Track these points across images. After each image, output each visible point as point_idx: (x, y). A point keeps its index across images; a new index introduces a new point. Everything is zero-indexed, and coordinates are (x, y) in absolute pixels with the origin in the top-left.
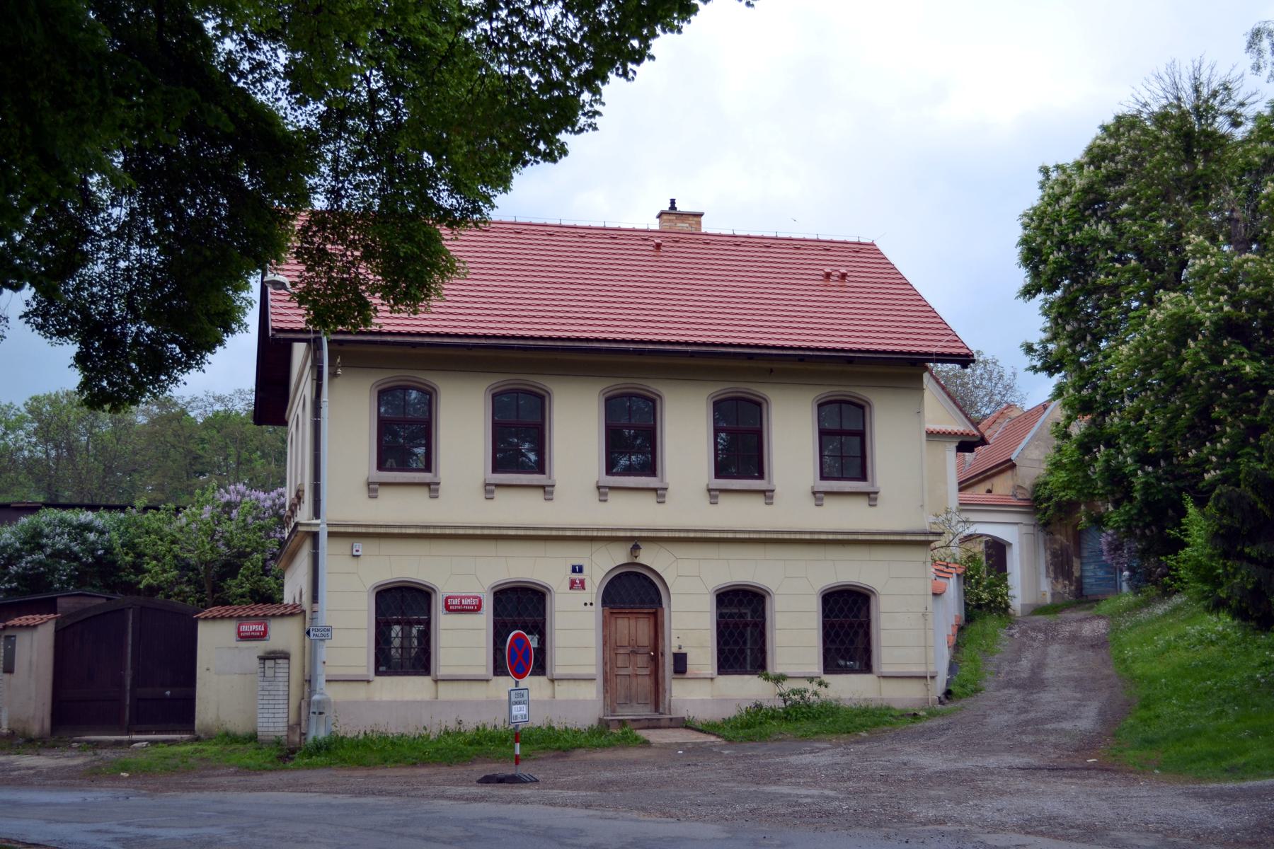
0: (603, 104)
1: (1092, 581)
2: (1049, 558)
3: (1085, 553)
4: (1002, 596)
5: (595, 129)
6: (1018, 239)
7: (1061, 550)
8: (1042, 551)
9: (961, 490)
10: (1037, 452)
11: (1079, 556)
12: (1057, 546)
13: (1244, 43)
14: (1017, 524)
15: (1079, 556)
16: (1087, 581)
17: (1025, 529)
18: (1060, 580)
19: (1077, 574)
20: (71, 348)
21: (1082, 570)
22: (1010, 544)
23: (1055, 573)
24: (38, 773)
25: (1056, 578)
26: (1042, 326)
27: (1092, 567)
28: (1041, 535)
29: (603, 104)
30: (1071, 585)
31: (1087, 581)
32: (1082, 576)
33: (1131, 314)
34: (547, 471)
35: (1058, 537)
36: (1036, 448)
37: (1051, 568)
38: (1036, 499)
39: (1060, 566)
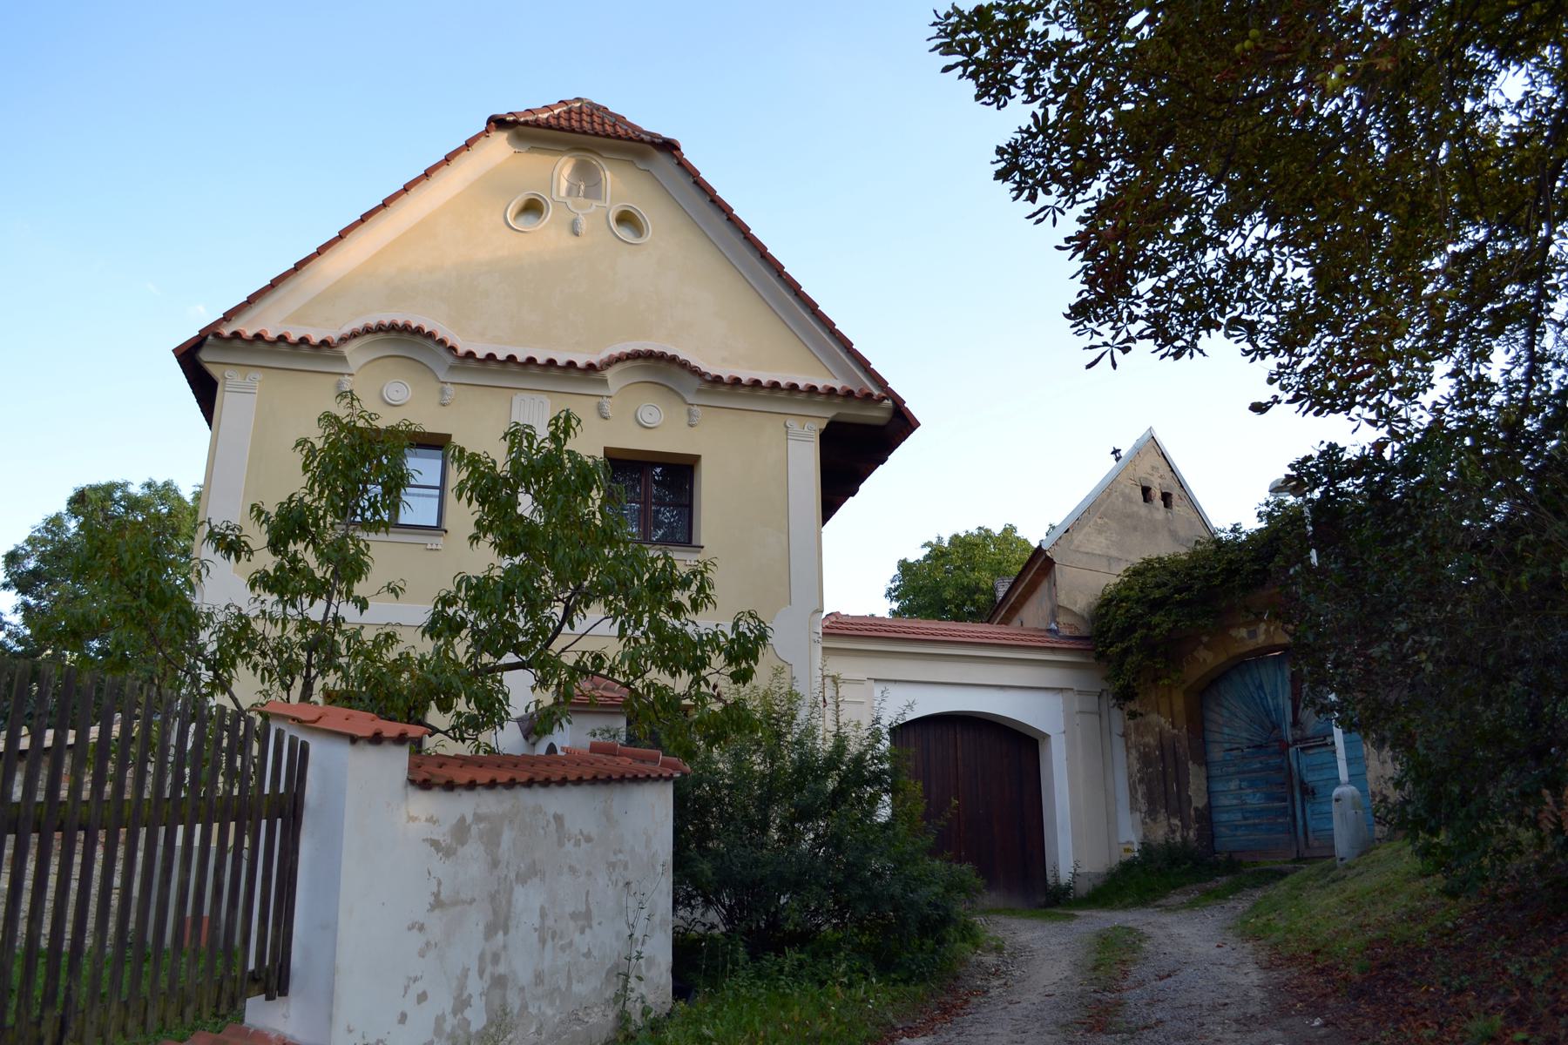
0: (960, 77)
1: (1237, 817)
2: (1136, 766)
3: (1216, 753)
4: (957, 978)
7: (1161, 747)
8: (1119, 744)
10: (1102, 540)
11: (1202, 759)
12: (1151, 740)
14: (1061, 690)
15: (1202, 759)
17: (1076, 703)
18: (1162, 817)
20: (426, 331)
21: (1210, 793)
22: (1046, 736)
23: (1151, 799)
24: (60, 875)
25: (1152, 813)
27: (1233, 785)
28: (1118, 719)
29: (960, 77)
30: (1185, 827)
31: (1224, 817)
32: (1209, 807)
34: (688, 463)
35: (1154, 718)
36: (1100, 532)
37: (1141, 790)
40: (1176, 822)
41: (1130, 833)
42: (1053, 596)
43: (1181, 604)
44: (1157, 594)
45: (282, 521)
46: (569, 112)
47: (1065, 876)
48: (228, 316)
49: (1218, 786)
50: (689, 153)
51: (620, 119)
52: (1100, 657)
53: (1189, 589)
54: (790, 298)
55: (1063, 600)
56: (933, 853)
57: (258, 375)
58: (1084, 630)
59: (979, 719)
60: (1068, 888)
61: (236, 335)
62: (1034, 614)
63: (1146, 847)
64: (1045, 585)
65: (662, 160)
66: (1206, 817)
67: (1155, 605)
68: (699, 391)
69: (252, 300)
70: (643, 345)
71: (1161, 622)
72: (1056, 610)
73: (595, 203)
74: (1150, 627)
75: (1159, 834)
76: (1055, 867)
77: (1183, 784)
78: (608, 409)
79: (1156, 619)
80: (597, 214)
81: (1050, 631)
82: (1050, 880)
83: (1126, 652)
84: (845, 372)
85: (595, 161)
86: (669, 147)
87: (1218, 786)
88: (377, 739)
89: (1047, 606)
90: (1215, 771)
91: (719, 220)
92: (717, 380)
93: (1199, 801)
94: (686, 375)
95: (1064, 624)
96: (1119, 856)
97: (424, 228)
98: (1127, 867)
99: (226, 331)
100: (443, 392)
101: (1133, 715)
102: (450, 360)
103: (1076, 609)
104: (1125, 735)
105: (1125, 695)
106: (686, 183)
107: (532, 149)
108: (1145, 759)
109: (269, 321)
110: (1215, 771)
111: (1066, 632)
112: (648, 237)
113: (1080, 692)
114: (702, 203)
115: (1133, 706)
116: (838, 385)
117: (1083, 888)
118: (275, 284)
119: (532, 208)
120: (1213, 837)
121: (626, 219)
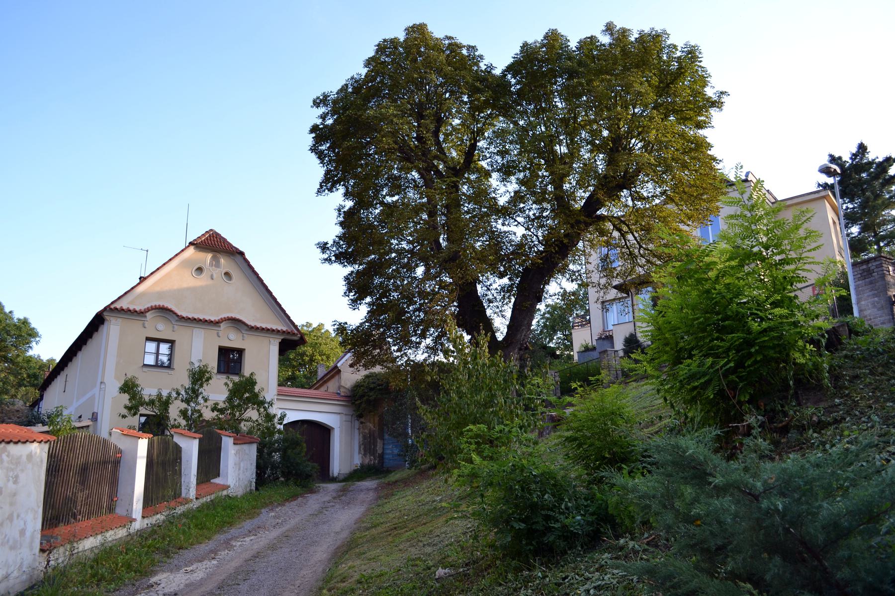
5: (831, 156)
6: (708, 61)
8: (357, 431)
9: (279, 385)
11: (382, 439)
12: (367, 431)
13: (449, 35)
15: (382, 439)
16: (387, 456)
17: (344, 418)
19: (380, 451)
22: (333, 428)
23: (365, 450)
25: (365, 455)
26: (15, 313)
27: (390, 447)
28: (357, 424)
30: (375, 459)
31: (387, 456)
32: (383, 453)
33: (572, 221)
35: (368, 424)
37: (362, 447)
38: (354, 396)
39: (368, 446)
40: (372, 457)
41: (357, 461)
42: (339, 381)
43: (380, 390)
44: (372, 386)
45: (18, 328)
46: (210, 236)
47: (336, 474)
48: (112, 303)
49: (386, 447)
50: (247, 256)
51: (225, 240)
52: (353, 403)
53: (382, 385)
54: (273, 302)
55: (343, 384)
56: (309, 460)
57: (120, 320)
58: (349, 394)
59: (323, 427)
60: (336, 477)
61: (116, 309)
62: (332, 386)
63: (362, 465)
64: (337, 377)
65: (239, 257)
66: (382, 456)
67: (371, 389)
68: (246, 330)
69: (119, 298)
70: (234, 315)
71: (373, 395)
72: (340, 387)
73: (219, 269)
74: (369, 396)
75: (367, 461)
76: (333, 471)
77: (375, 446)
78: (220, 334)
79: (371, 394)
80: (218, 273)
81: (338, 393)
82: (331, 475)
83: (361, 403)
84: (288, 326)
85: (219, 255)
86: (242, 254)
87: (386, 447)
88: (230, 437)
89: (337, 384)
90: (386, 442)
91: (255, 277)
92: (252, 328)
93: (380, 451)
94: (243, 326)
95: (342, 392)
96: (354, 468)
97: (168, 275)
98: (355, 471)
99: (112, 307)
100: (173, 327)
101: (362, 423)
102: (177, 318)
103: (347, 387)
104: (359, 429)
105: (360, 416)
106: (245, 265)
107: (200, 251)
108: (364, 437)
109: (124, 304)
110: (386, 442)
111: (343, 394)
112: (234, 280)
113: (346, 415)
114: (250, 271)
115: (362, 420)
116: (284, 329)
117: (341, 477)
118: (126, 293)
119: (200, 270)
120: (383, 463)
121: (227, 274)
